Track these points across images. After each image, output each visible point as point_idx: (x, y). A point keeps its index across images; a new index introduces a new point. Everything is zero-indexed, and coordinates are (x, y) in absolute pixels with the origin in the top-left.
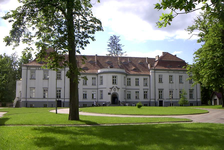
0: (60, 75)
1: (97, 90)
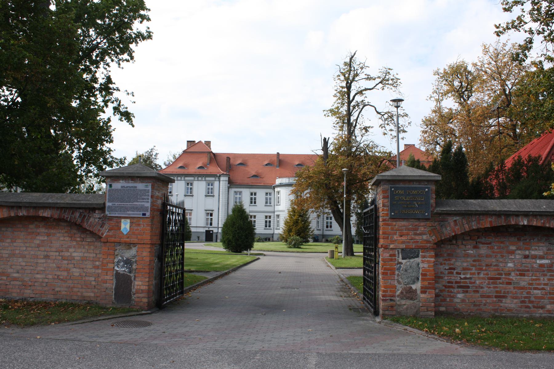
0: (191, 189)
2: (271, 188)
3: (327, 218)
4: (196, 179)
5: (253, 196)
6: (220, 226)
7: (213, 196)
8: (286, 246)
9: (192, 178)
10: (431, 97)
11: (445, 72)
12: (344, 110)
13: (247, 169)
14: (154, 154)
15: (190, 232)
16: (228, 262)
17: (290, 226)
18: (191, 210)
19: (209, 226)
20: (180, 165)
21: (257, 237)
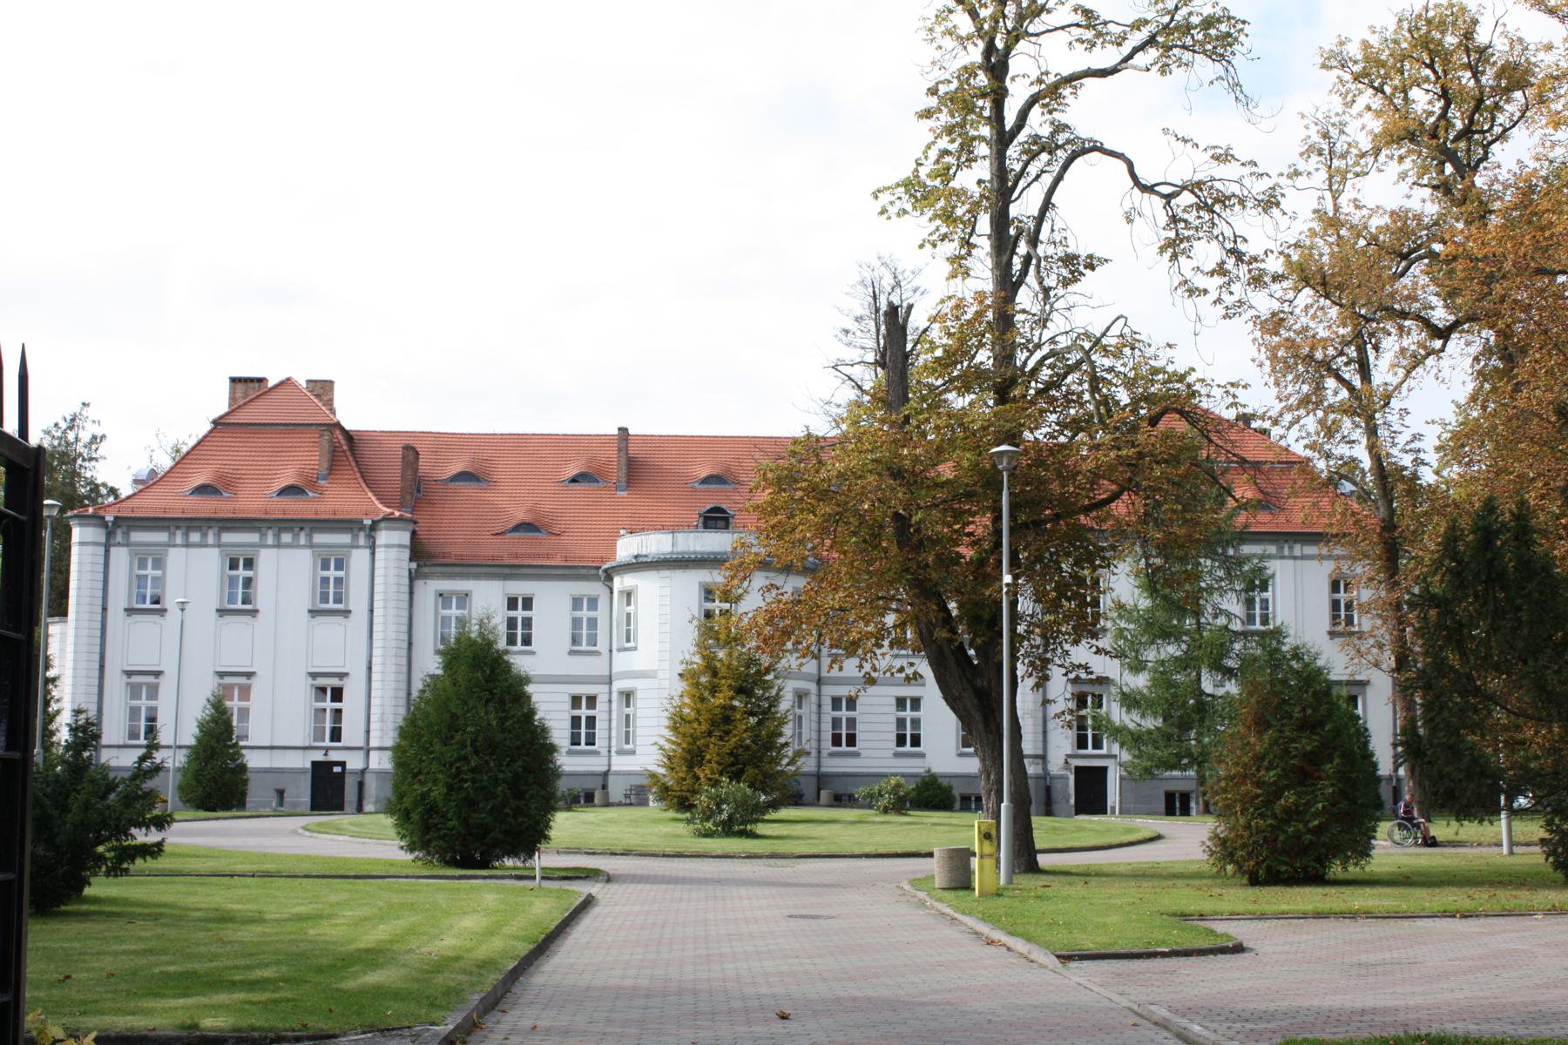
0: (248, 582)
1: (605, 688)
2: (596, 578)
3: (836, 703)
4: (270, 540)
5: (520, 614)
6: (374, 743)
7: (346, 613)
8: (682, 828)
9: (253, 537)
10: (1297, 173)
11: (1367, 59)
12: (973, 177)
13: (490, 496)
14: (85, 437)
15: (243, 768)
16: (447, 944)
17: (695, 739)
18: (249, 675)
19: (327, 743)
20: (200, 479)
21: (562, 786)
